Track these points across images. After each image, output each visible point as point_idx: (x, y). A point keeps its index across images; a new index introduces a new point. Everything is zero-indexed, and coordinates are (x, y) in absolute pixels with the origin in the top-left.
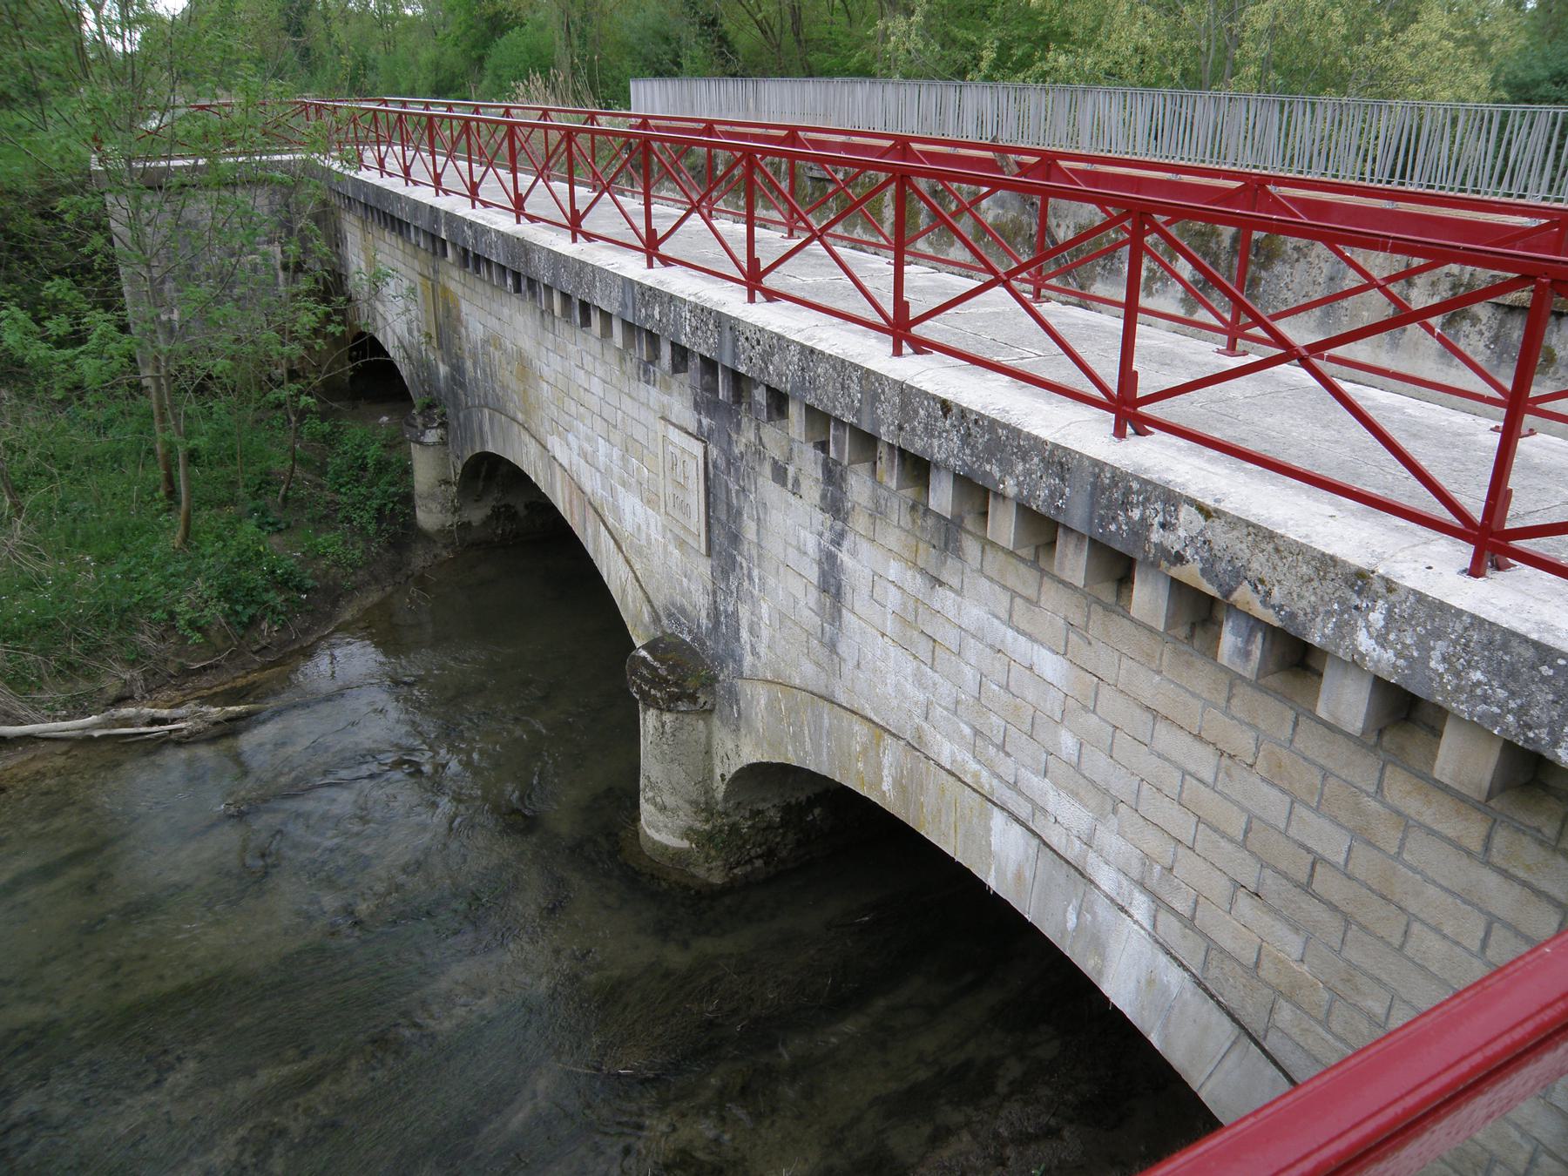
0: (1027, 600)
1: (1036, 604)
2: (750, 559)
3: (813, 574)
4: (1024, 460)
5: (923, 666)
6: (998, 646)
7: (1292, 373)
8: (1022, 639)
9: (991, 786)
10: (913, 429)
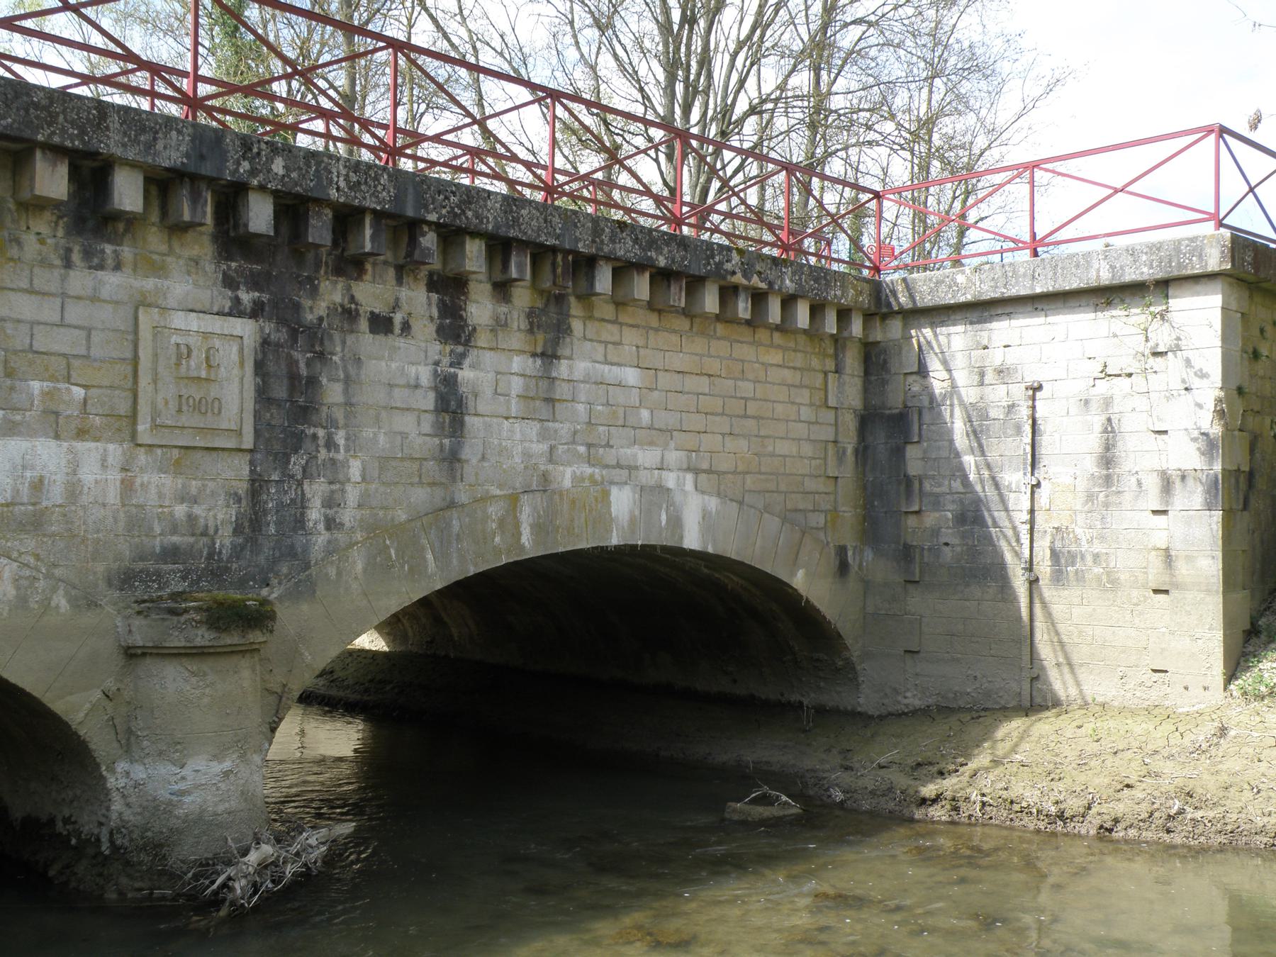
0: (614, 343)
1: (620, 343)
2: (332, 423)
3: (428, 401)
4: (668, 246)
5: (546, 423)
6: (599, 381)
7: (1119, 186)
8: (614, 368)
9: (602, 476)
10: (602, 241)
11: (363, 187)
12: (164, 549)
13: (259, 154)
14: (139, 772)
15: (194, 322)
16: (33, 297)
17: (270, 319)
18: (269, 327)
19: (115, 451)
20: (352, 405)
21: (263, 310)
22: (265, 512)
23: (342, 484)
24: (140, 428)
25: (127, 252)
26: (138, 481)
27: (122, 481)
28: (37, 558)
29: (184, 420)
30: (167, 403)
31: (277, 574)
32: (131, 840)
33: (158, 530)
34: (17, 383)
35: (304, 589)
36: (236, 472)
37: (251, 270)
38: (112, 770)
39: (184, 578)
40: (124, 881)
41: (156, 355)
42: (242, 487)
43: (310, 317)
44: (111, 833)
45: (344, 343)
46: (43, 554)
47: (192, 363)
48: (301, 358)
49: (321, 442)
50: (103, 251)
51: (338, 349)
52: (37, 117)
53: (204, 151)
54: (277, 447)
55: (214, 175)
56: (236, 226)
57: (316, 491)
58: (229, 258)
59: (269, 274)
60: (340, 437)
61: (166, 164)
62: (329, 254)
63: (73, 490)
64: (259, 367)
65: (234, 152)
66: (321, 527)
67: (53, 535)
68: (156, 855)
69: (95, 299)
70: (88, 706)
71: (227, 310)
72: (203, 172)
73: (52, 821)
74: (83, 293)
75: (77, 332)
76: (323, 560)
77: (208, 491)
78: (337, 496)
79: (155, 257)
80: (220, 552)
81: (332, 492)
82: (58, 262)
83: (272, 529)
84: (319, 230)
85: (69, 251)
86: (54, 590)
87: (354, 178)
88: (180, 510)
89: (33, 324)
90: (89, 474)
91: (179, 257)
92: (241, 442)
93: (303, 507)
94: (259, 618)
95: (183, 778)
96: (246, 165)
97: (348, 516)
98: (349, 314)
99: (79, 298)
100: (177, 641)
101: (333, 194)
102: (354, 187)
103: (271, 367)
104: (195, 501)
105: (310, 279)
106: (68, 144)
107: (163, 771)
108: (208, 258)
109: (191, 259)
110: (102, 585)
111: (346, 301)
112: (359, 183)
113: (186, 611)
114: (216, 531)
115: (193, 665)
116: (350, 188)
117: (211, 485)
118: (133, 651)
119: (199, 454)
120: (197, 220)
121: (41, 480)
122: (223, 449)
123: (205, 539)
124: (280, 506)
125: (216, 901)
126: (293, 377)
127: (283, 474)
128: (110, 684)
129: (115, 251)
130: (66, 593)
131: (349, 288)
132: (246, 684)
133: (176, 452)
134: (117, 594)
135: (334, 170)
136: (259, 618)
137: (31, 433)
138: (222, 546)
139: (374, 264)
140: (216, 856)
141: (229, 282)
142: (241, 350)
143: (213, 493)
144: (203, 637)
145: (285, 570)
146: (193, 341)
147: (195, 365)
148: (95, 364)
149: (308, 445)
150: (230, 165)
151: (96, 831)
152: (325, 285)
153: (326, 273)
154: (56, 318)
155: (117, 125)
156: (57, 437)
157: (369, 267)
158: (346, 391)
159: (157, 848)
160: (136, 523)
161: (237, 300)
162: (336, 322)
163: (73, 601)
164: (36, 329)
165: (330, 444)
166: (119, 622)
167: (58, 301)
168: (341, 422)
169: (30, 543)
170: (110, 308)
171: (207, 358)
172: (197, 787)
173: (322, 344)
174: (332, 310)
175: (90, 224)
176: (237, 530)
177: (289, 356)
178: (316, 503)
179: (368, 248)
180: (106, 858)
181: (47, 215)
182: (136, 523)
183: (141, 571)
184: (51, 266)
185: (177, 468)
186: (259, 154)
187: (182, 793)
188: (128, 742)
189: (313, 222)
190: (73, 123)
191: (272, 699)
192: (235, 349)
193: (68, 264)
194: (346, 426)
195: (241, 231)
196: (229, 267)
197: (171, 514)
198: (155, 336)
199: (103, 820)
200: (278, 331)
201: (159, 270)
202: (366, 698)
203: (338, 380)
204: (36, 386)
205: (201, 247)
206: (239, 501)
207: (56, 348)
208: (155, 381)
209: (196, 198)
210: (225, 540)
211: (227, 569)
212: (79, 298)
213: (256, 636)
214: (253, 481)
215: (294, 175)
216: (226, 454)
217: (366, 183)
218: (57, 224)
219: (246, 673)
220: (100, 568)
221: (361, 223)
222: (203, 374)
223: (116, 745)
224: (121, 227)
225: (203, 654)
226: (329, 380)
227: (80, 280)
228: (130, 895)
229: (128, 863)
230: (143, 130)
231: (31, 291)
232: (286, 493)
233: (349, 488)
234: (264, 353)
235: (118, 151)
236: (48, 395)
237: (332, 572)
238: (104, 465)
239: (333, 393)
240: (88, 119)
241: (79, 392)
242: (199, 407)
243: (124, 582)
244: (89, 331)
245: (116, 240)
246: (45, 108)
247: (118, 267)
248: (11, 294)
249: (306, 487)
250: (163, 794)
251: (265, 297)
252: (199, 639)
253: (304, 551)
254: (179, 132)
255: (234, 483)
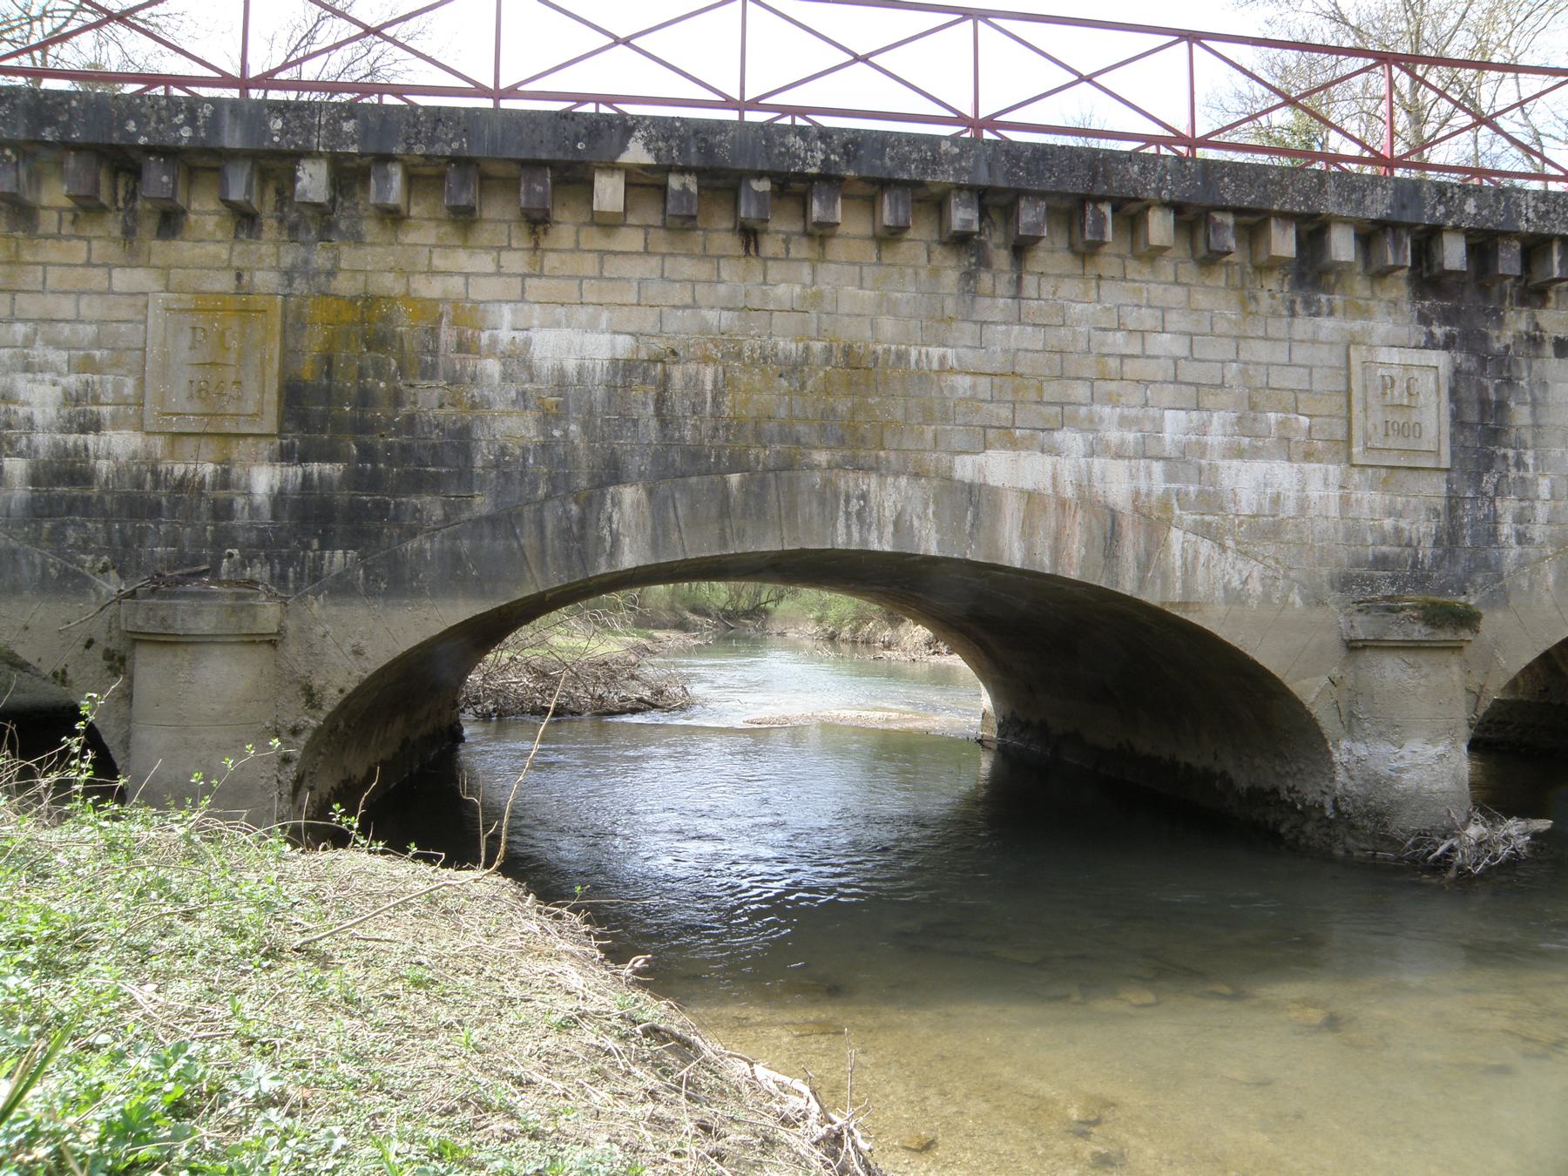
2: (1521, 445)
11: (1552, 216)
12: (1375, 557)
13: (1452, 197)
14: (1361, 750)
15: (1396, 356)
16: (1268, 343)
17: (1461, 350)
18: (1460, 357)
19: (1334, 471)
20: (1539, 426)
21: (1454, 342)
22: (1462, 526)
23: (1532, 501)
24: (1355, 450)
25: (1338, 299)
26: (1353, 496)
27: (1341, 497)
28: (1277, 562)
29: (1391, 443)
30: (1375, 428)
31: (1473, 584)
32: (1355, 808)
33: (1370, 540)
34: (1259, 415)
35: (1500, 597)
36: (1435, 489)
37: (1442, 307)
38: (1336, 746)
39: (1393, 584)
40: (1350, 841)
41: (1365, 386)
42: (1441, 504)
43: (1497, 346)
44: (1335, 801)
45: (1530, 368)
46: (1281, 558)
47: (1396, 393)
48: (1491, 384)
49: (1511, 462)
50: (1319, 301)
51: (1525, 374)
52: (1273, 191)
53: (1405, 201)
54: (1471, 467)
55: (1415, 221)
56: (1429, 267)
57: (1507, 507)
58: (1423, 298)
59: (1458, 310)
60: (1529, 458)
61: (1374, 216)
62: (1513, 286)
63: (1303, 505)
64: (1453, 393)
65: (1430, 200)
66: (1513, 541)
67: (1288, 543)
68: (1378, 822)
69: (1314, 341)
70: (1318, 689)
71: (1422, 344)
72: (1405, 220)
73: (1275, 791)
74: (1305, 337)
75: (1302, 370)
76: (1514, 572)
77: (1411, 507)
78: (1528, 513)
79: (1361, 302)
80: (1423, 562)
81: (1523, 508)
82: (1285, 313)
83: (1468, 543)
84: (1508, 261)
85: (1293, 302)
86: (1291, 589)
87: (1542, 208)
88: (1388, 523)
89: (992, 402)
90: (1315, 491)
91: (1381, 300)
92: (1439, 462)
93: (1496, 523)
94: (1467, 619)
95: (1402, 757)
96: (1441, 209)
97: (1538, 532)
98: (1534, 341)
99: (1302, 341)
100: (1396, 635)
101: (1523, 225)
102: (1543, 216)
103: (1463, 393)
104: (1400, 515)
105: (1496, 311)
106: (1296, 209)
107: (1383, 750)
108: (1405, 299)
109: (1390, 301)
110: (1326, 587)
111: (1531, 328)
112: (1548, 212)
113: (1402, 609)
114: (1419, 542)
115: (1410, 658)
116: (1540, 218)
117: (1413, 501)
118: (1354, 644)
119: (1403, 474)
120: (1400, 264)
121: (1278, 495)
122: (1423, 469)
123: (1410, 550)
124: (1475, 521)
125: (1443, 863)
126: (1484, 403)
127: (1477, 492)
128: (1335, 672)
129: (1328, 300)
130: (1300, 592)
131: (1533, 317)
132: (1456, 678)
133: (1383, 471)
134: (1338, 595)
135: (1523, 203)
136: (1467, 619)
137: (1270, 457)
138: (1424, 556)
139: (1558, 292)
140: (1433, 829)
141: (1424, 319)
142: (1437, 379)
143: (1416, 509)
144: (1419, 632)
145: (1480, 580)
146: (1395, 372)
147: (1398, 394)
148: (1318, 397)
149: (1499, 465)
150: (1428, 210)
151: (1320, 799)
152: (1510, 316)
153: (1511, 304)
154: (1285, 359)
155: (1333, 189)
156: (1289, 459)
157: (1552, 295)
158: (1533, 414)
159: (1379, 816)
160: (1353, 534)
161: (1431, 335)
162: (1522, 349)
163: (1304, 598)
164: (1271, 369)
165: (1520, 464)
166: (1341, 619)
167: (1287, 345)
168: (1530, 443)
169: (1271, 549)
170: (1326, 348)
171: (1408, 387)
172: (1415, 766)
173: (1509, 370)
174: (1518, 338)
175: (1309, 279)
176: (1437, 542)
177: (1479, 383)
178: (1508, 518)
179: (1556, 273)
180: (1331, 821)
181: (1276, 275)
182: (1353, 534)
183: (1358, 576)
184: (1280, 316)
185: (1385, 486)
186: (1452, 197)
187: (1401, 770)
188: (1351, 724)
189: (1502, 254)
190: (1299, 192)
191: (1472, 697)
192: (1432, 378)
193: (1293, 314)
194: (1534, 446)
195: (1436, 270)
196: (1423, 306)
197: (1381, 526)
198: (1364, 369)
199: (1326, 790)
200: (1468, 360)
201: (1364, 313)
202: (1487, 735)
203: (1525, 404)
204: (1273, 417)
205: (1399, 289)
206: (1438, 515)
207: (1286, 384)
208: (1365, 410)
209: (1397, 244)
210: (1426, 551)
211: (1429, 577)
212: (1302, 341)
213: (1465, 634)
214: (1450, 498)
215: (1485, 212)
216: (1426, 473)
217: (1555, 211)
218: (1283, 280)
219: (1455, 669)
220: (1325, 572)
221: (1547, 253)
222: (1405, 402)
223: (1339, 725)
224: (1332, 278)
225: (1419, 648)
226: (1517, 404)
227: (1303, 326)
228: (1356, 854)
229: (1353, 826)
230: (1354, 190)
231: (1266, 338)
232: (1480, 508)
233: (1538, 504)
234: (1456, 381)
235: (1334, 210)
236: (1282, 424)
237: (1525, 583)
238: (1326, 484)
239: (1521, 415)
240: (1311, 187)
241: (1304, 421)
242: (1405, 430)
243: (1344, 585)
244: (1311, 368)
245: (1329, 290)
246: (1278, 183)
247: (1331, 313)
248: (1251, 341)
249: (1498, 503)
250: (1384, 770)
251: (1456, 330)
252: (1416, 634)
253: (1497, 564)
254: (1384, 187)
255: (1433, 500)
